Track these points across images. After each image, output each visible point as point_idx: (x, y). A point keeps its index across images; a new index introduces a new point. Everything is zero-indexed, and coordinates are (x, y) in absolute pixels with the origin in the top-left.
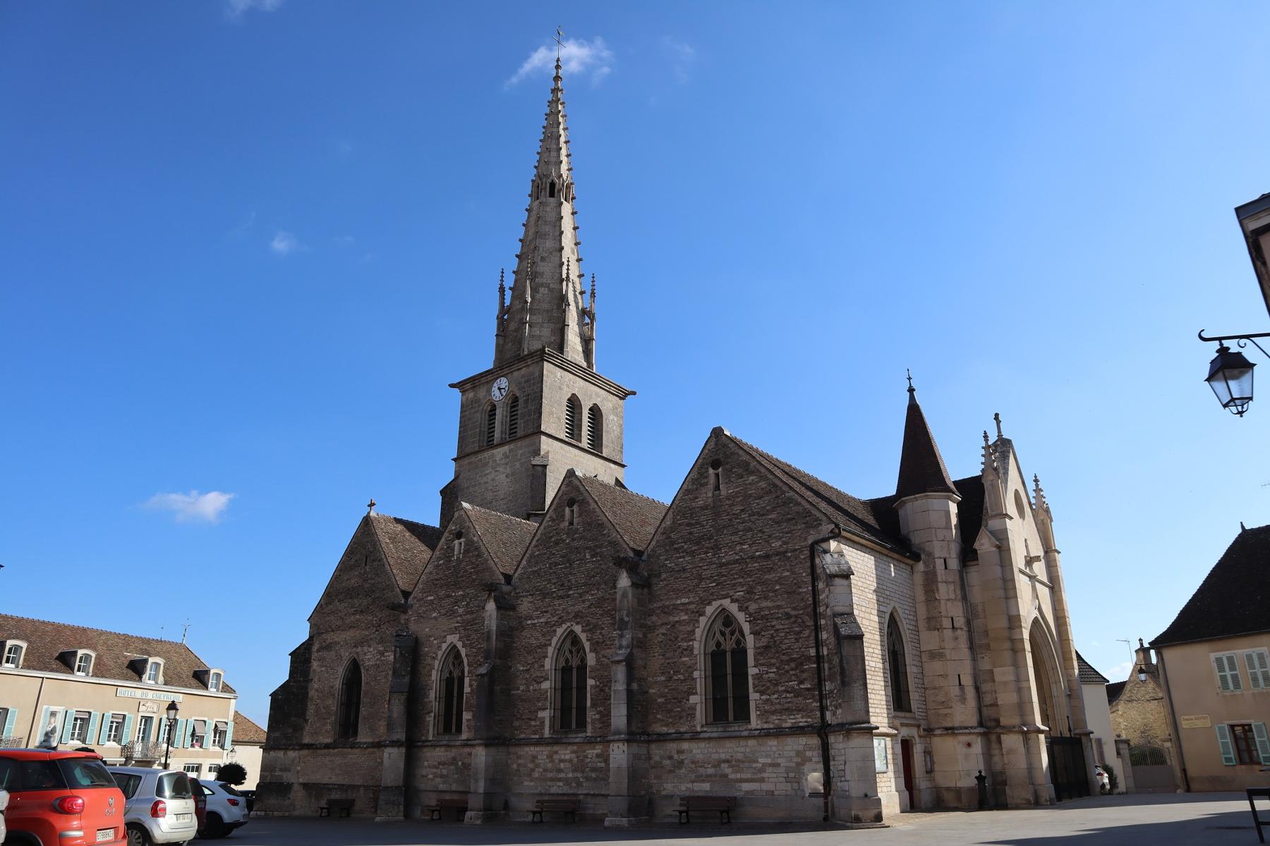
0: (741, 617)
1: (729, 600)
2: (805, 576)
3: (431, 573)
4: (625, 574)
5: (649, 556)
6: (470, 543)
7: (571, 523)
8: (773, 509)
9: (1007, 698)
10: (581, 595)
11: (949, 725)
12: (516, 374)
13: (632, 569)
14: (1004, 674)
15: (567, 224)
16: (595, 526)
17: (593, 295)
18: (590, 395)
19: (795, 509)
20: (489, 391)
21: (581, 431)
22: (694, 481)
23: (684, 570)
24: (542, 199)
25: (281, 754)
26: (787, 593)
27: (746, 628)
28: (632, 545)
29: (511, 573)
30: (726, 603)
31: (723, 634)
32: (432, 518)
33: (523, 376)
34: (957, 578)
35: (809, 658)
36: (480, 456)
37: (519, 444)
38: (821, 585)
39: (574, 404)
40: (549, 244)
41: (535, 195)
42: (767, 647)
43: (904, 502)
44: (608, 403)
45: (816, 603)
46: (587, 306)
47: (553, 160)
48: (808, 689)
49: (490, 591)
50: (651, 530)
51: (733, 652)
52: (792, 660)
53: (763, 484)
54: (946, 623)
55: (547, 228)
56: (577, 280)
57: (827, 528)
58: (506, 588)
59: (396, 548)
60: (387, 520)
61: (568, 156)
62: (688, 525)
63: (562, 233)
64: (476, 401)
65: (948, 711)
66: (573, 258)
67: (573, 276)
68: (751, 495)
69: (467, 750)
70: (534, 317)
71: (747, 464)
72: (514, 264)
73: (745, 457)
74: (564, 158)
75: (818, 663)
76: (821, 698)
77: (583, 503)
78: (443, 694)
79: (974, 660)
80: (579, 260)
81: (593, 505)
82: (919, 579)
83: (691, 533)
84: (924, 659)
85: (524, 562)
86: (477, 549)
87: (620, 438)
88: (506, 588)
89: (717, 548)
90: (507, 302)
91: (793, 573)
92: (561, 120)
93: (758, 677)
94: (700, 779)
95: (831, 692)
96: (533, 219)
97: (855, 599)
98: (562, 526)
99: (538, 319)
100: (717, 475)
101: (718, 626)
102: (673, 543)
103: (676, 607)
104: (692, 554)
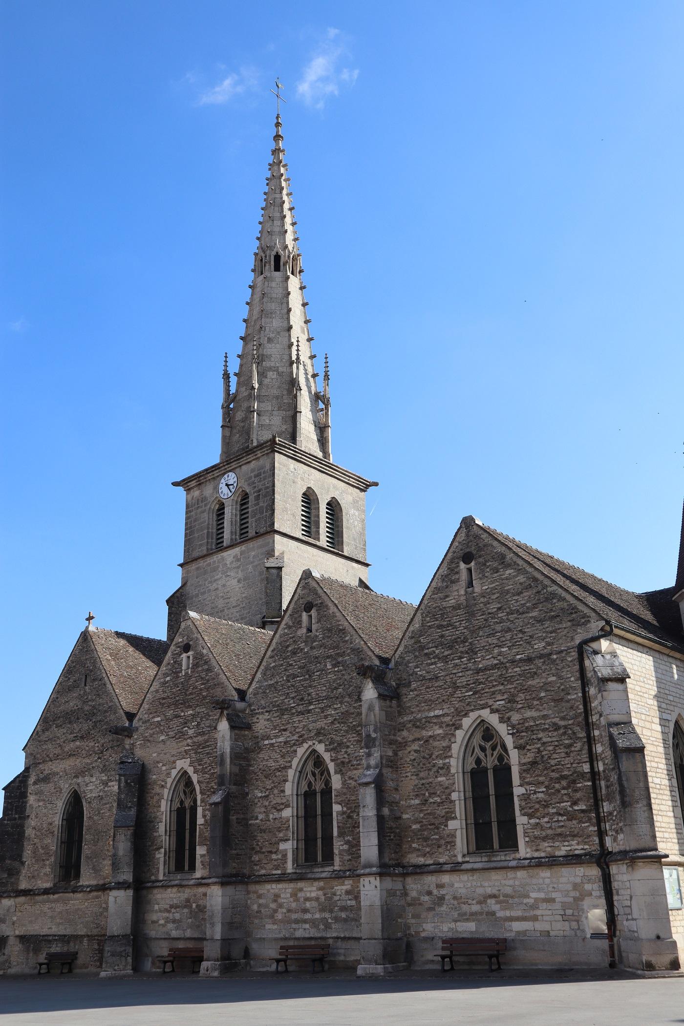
0: (502, 729)
1: (488, 710)
3: (157, 691)
5: (397, 663)
7: (309, 630)
8: (535, 606)
10: (323, 710)
13: (379, 679)
15: (295, 300)
16: (337, 632)
18: (327, 488)
19: (560, 604)
20: (216, 489)
22: (444, 578)
23: (437, 678)
24: (267, 273)
26: (554, 700)
27: (509, 741)
28: (377, 651)
29: (244, 688)
30: (485, 713)
31: (483, 749)
32: (156, 629)
33: (253, 470)
35: (582, 775)
36: (209, 560)
37: (251, 544)
38: (592, 691)
39: (309, 499)
40: (277, 323)
42: (534, 763)
44: (347, 496)
46: (320, 389)
47: (277, 229)
48: (583, 811)
49: (222, 709)
51: (495, 769)
52: (563, 777)
53: (521, 578)
55: (273, 306)
56: (308, 362)
58: (240, 705)
60: (107, 634)
62: (440, 627)
63: (289, 310)
64: (203, 499)
66: (303, 338)
67: (304, 357)
69: (201, 890)
70: (262, 405)
73: (501, 549)
74: (289, 227)
76: (599, 821)
77: (322, 606)
80: (310, 340)
81: (333, 609)
83: (442, 636)
87: (362, 534)
88: (240, 705)
89: (472, 652)
90: (233, 390)
91: (560, 677)
92: (284, 184)
93: (525, 798)
94: (464, 917)
99: (267, 406)
100: (470, 570)
101: (477, 740)
102: (422, 648)
103: (428, 720)
104: (445, 660)
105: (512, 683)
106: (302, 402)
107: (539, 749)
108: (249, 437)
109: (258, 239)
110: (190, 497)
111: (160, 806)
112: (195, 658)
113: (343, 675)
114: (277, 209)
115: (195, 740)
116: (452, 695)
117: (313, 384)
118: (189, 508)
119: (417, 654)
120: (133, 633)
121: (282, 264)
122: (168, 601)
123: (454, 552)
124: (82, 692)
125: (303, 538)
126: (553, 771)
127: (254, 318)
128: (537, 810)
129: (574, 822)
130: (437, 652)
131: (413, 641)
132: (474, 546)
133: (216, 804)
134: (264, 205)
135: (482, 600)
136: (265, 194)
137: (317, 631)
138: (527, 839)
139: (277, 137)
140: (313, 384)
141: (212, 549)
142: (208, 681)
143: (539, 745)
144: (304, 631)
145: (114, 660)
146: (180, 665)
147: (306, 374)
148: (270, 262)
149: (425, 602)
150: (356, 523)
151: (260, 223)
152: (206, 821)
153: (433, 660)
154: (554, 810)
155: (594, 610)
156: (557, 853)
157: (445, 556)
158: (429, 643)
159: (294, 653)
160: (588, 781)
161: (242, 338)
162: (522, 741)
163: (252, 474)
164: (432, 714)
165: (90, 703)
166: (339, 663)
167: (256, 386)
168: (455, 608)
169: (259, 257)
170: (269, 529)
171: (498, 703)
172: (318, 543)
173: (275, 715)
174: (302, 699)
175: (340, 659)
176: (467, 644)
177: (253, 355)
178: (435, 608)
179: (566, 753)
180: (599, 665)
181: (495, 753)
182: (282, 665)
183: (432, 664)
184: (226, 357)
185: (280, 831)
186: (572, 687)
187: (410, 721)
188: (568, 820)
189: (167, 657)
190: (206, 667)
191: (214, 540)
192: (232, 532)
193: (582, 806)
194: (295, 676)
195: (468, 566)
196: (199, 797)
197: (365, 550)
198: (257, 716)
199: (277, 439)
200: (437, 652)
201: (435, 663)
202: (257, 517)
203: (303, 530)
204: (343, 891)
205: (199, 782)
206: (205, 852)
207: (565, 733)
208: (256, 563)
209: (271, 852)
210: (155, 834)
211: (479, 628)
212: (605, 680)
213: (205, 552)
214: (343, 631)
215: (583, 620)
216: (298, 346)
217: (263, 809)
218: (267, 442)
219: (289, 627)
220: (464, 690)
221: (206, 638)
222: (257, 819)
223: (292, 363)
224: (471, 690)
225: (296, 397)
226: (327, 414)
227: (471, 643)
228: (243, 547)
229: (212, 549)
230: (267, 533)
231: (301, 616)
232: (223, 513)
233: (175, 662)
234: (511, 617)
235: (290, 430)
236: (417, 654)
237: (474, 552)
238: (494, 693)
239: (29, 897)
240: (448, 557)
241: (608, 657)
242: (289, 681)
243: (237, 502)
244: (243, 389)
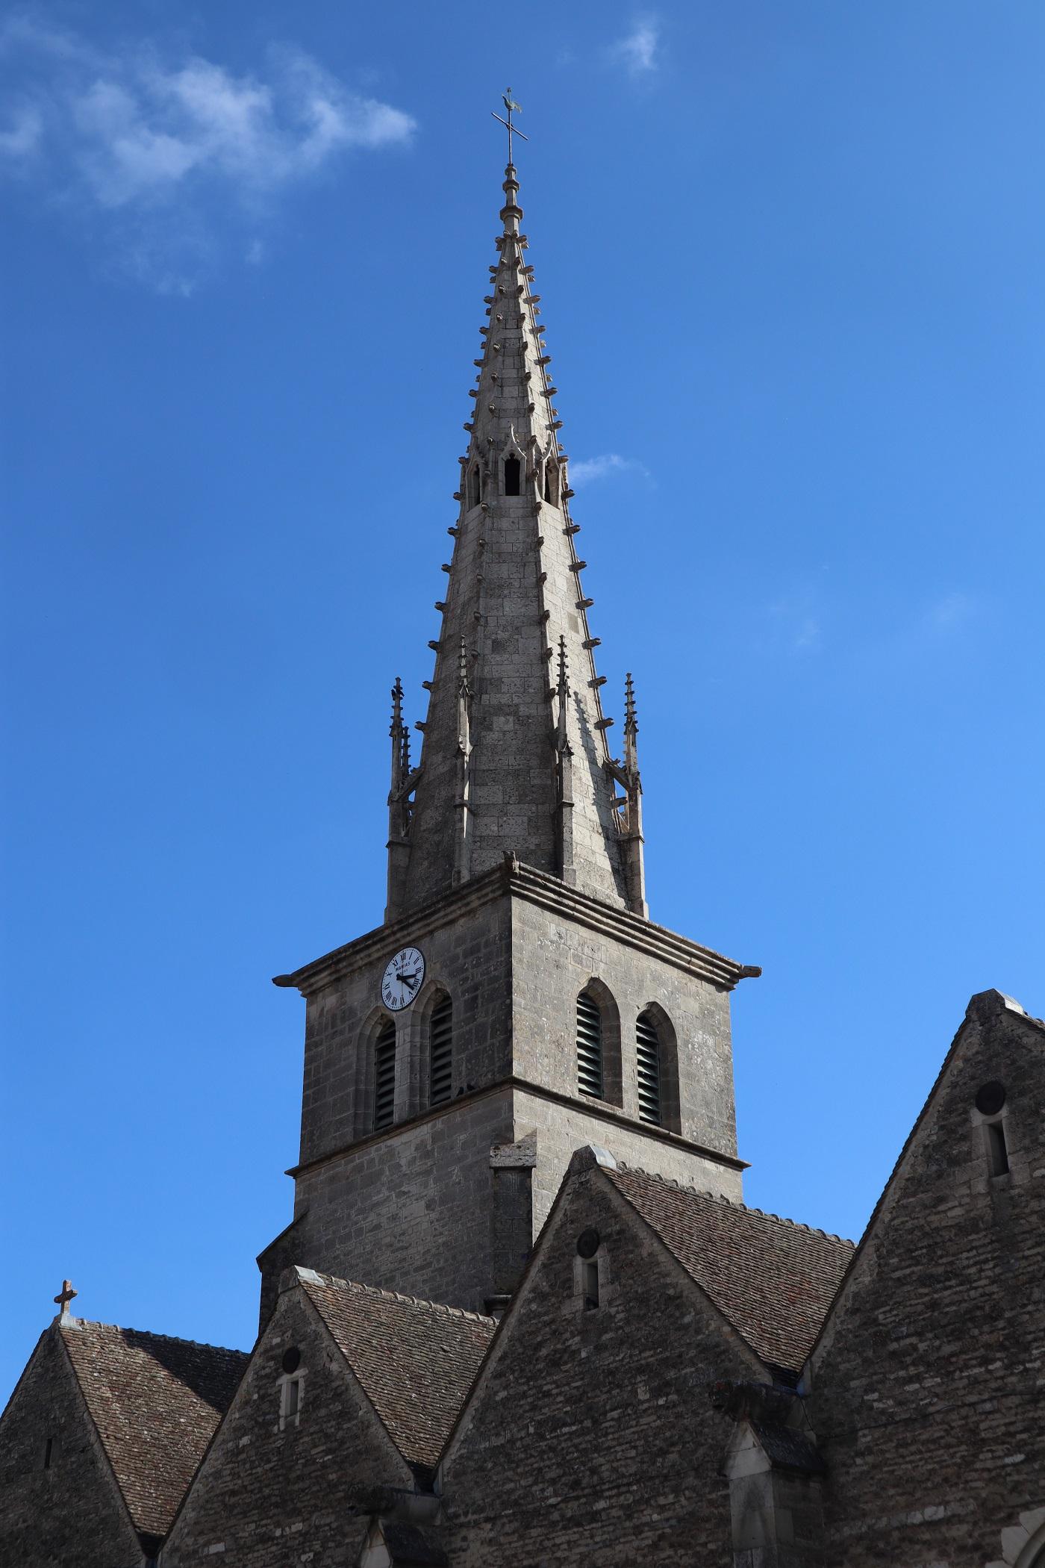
3: (217, 1475)
4: (749, 1439)
5: (817, 1380)
6: (321, 1380)
7: (592, 1302)
10: (629, 1511)
12: (441, 936)
13: (772, 1424)
15: (555, 556)
16: (660, 1306)
17: (631, 727)
18: (639, 981)
20: (376, 988)
21: (618, 1074)
22: (930, 1152)
23: (923, 1417)
24: (490, 500)
28: (764, 1350)
29: (429, 1459)
32: (232, 1323)
33: (460, 941)
36: (360, 1158)
37: (457, 1116)
39: (596, 1005)
40: (512, 608)
41: (471, 493)
44: (686, 1000)
46: (618, 755)
47: (511, 405)
49: (373, 1512)
50: (817, 1310)
55: (504, 571)
56: (588, 694)
58: (420, 1504)
59: (128, 1412)
60: (104, 1336)
61: (547, 393)
62: (927, 1280)
63: (542, 578)
64: (346, 1013)
66: (575, 641)
67: (579, 683)
70: (481, 792)
72: (427, 665)
74: (539, 402)
77: (622, 1241)
80: (589, 644)
81: (649, 1245)
83: (934, 1305)
85: (467, 1424)
86: (339, 1395)
87: (724, 1091)
88: (420, 1504)
89: (1016, 1345)
90: (415, 762)
92: (524, 308)
96: (468, 552)
98: (566, 1311)
99: (494, 794)
100: (997, 1130)
102: (882, 1338)
104: (944, 1366)
106: (575, 783)
108: (452, 866)
109: (469, 427)
110: (315, 1010)
112: (311, 1384)
113: (679, 1416)
114: (509, 361)
116: (968, 1463)
117: (598, 744)
119: (870, 1354)
120: (171, 1334)
121: (522, 477)
122: (260, 1260)
123: (954, 1085)
124: (38, 1484)
125: (583, 1099)
127: (462, 599)
130: (922, 1346)
131: (857, 1320)
134: (481, 355)
136: (483, 331)
137: (610, 1303)
139: (509, 212)
140: (598, 744)
141: (366, 1132)
142: (342, 1442)
144: (579, 1304)
145: (119, 1399)
146: (275, 1403)
147: (583, 720)
148: (496, 475)
149: (886, 1216)
150: (710, 1065)
151: (473, 393)
153: (912, 1371)
157: (932, 1096)
158: (900, 1324)
159: (555, 1363)
161: (433, 645)
163: (459, 950)
164: (917, 1518)
165: (56, 1512)
166: (667, 1384)
167: (468, 748)
169: (471, 466)
170: (499, 1078)
172: (619, 1112)
173: (508, 1528)
174: (576, 1484)
175: (672, 1374)
176: (1001, 1324)
177: (460, 678)
178: (911, 1231)
182: (524, 1395)
183: (910, 1380)
187: (860, 1538)
189: (244, 1385)
190: (337, 1407)
191: (372, 1111)
192: (412, 1089)
194: (557, 1424)
195: (992, 1119)
197: (732, 1129)
198: (464, 1532)
199: (516, 864)
200: (922, 1346)
201: (918, 1378)
203: (581, 1080)
208: (469, 1161)
211: (1031, 1281)
213: (350, 1139)
214: (675, 1302)
216: (562, 655)
218: (493, 871)
219: (540, 1296)
220: (1000, 1450)
221: (337, 1332)
223: (549, 695)
224: (1018, 1448)
225: (559, 770)
226: (634, 810)
227: (1011, 1322)
228: (439, 1124)
229: (366, 1132)
230: (495, 1086)
231: (570, 1267)
232: (393, 1046)
233: (262, 1398)
235: (548, 847)
236: (870, 1354)
237: (1007, 1082)
240: (940, 1099)
242: (542, 1437)
243: (423, 1017)
244: (439, 758)
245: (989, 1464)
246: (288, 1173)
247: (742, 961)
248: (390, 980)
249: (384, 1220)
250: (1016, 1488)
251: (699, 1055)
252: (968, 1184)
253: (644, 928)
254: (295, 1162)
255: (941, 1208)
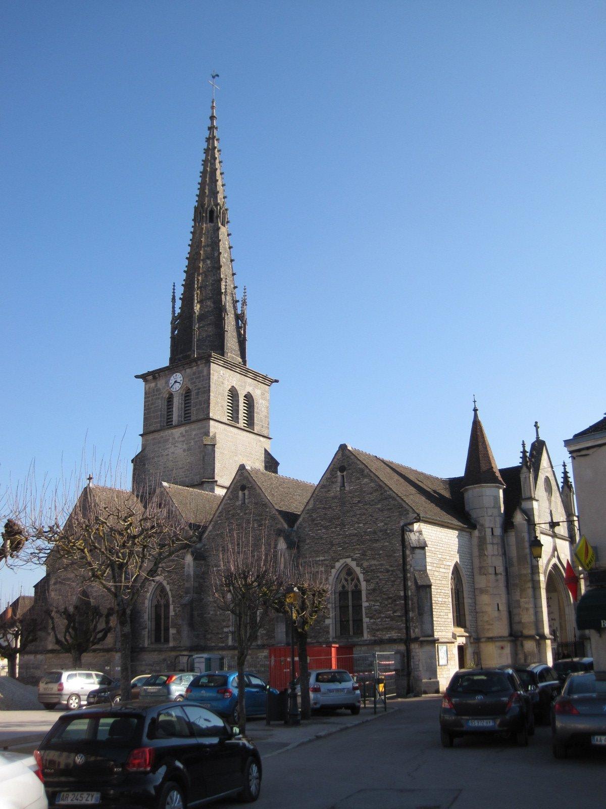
0: (358, 570)
1: (350, 559)
2: (398, 546)
7: (244, 503)
9: (527, 618)
11: (491, 635)
14: (526, 602)
18: (246, 385)
19: (393, 502)
20: (167, 383)
22: (327, 479)
25: (31, 657)
26: (387, 556)
27: (361, 577)
30: (349, 560)
31: (346, 580)
34: (499, 541)
35: (400, 598)
36: (162, 434)
37: (193, 426)
38: (408, 552)
42: (374, 590)
43: (467, 490)
45: (405, 563)
48: (399, 616)
51: (353, 592)
54: (491, 570)
57: (412, 516)
65: (491, 627)
68: (365, 492)
71: (362, 471)
73: (362, 466)
75: (405, 601)
76: (407, 621)
78: (153, 616)
79: (508, 593)
82: (475, 541)
84: (476, 593)
89: (343, 525)
91: (391, 543)
95: (413, 618)
97: (428, 560)
101: (343, 575)
102: (313, 520)
103: (317, 562)
104: (326, 528)
105: (364, 544)
107: (377, 582)
111: (144, 603)
115: (167, 564)
116: (330, 549)
118: (147, 394)
119: (310, 523)
123: (334, 465)
126: (384, 594)
128: (375, 615)
129: (394, 622)
132: (345, 463)
133: (185, 605)
135: (350, 495)
138: (368, 630)
143: (378, 580)
149: (316, 493)
152: (176, 614)
153: (320, 528)
154: (384, 615)
155: (411, 508)
156: (384, 638)
160: (403, 600)
162: (368, 577)
168: (333, 498)
171: (356, 555)
176: (340, 520)
179: (392, 585)
180: (413, 538)
181: (353, 583)
183: (319, 530)
184: (174, 286)
185: (224, 622)
186: (397, 549)
188: (391, 620)
191: (165, 419)
192: (179, 416)
193: (398, 614)
196: (171, 599)
201: (321, 530)
202: (198, 407)
204: (263, 656)
205: (170, 590)
206: (175, 632)
207: (391, 575)
208: (197, 439)
209: (218, 633)
210: (141, 620)
212: (414, 548)
213: (159, 428)
214: (265, 505)
215: (405, 513)
217: (213, 609)
222: (209, 614)
224: (341, 547)
234: (366, 507)
236: (310, 523)
238: (354, 549)
239: (55, 654)
241: (417, 534)
243: (182, 395)
245: (334, 549)
246: (140, 435)
247: (274, 378)
248: (172, 381)
249: (170, 453)
250: (339, 555)
251: (261, 405)
252: (335, 488)
253: (248, 371)
254: (142, 433)
255: (329, 492)
